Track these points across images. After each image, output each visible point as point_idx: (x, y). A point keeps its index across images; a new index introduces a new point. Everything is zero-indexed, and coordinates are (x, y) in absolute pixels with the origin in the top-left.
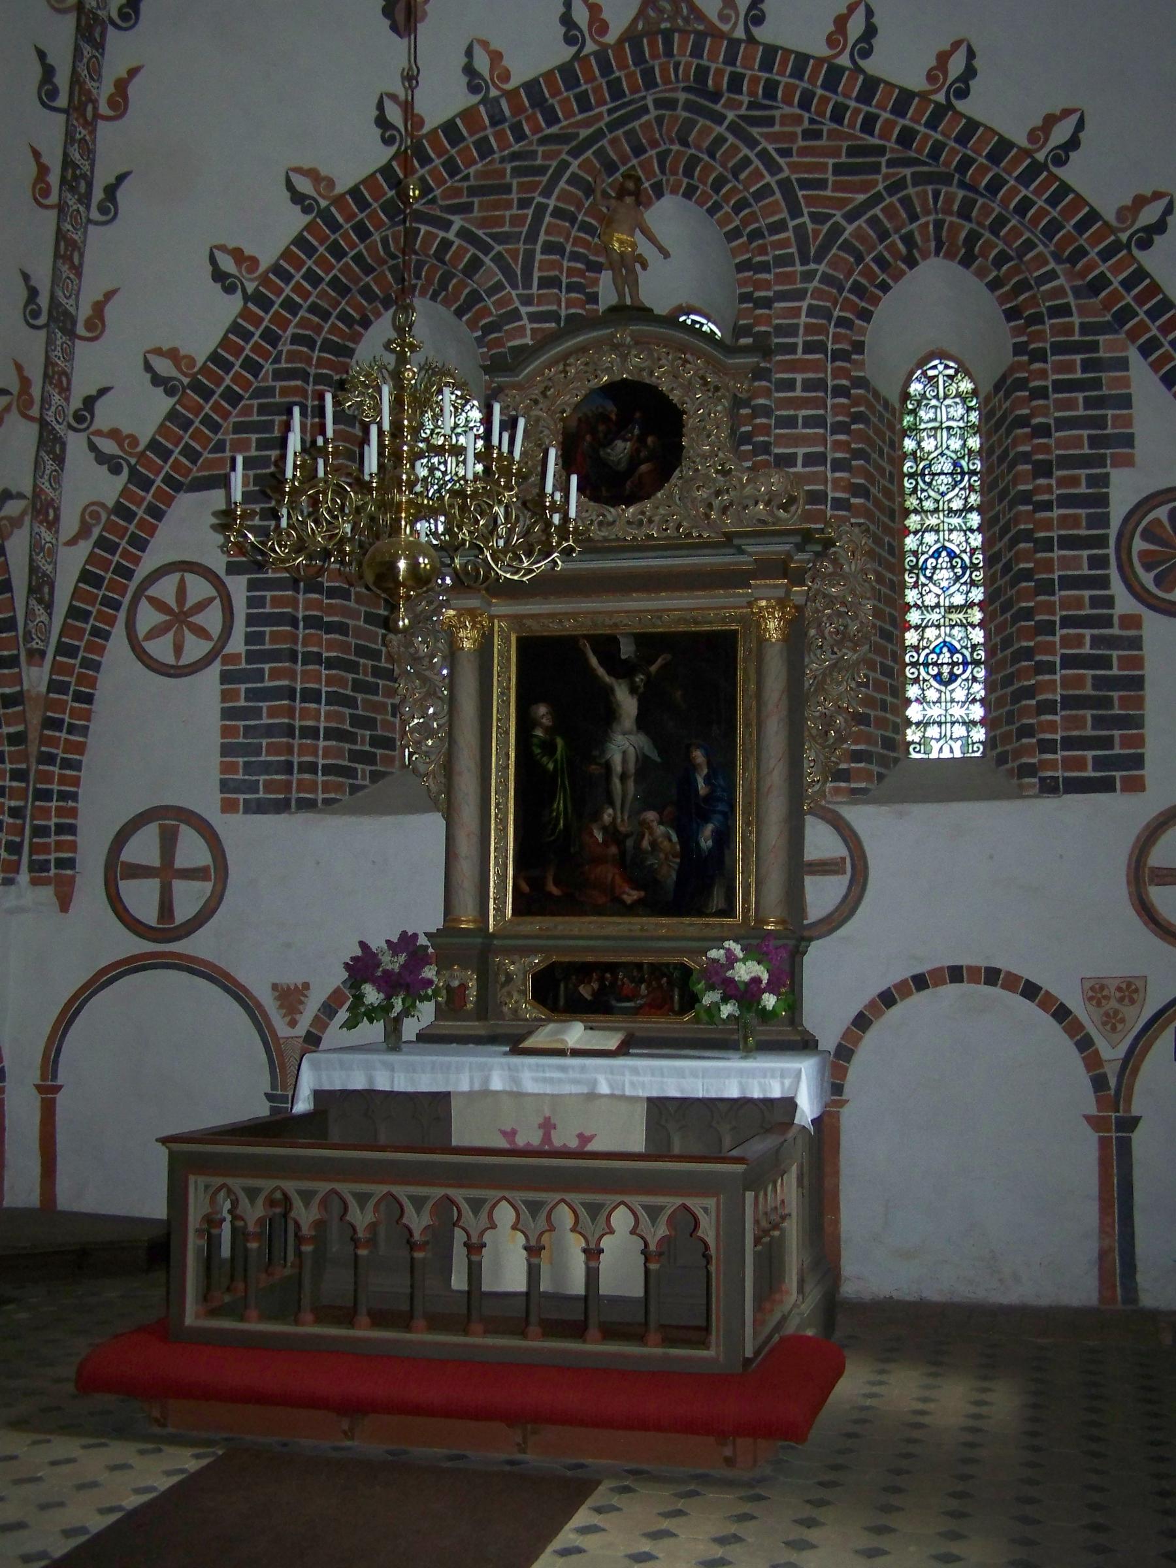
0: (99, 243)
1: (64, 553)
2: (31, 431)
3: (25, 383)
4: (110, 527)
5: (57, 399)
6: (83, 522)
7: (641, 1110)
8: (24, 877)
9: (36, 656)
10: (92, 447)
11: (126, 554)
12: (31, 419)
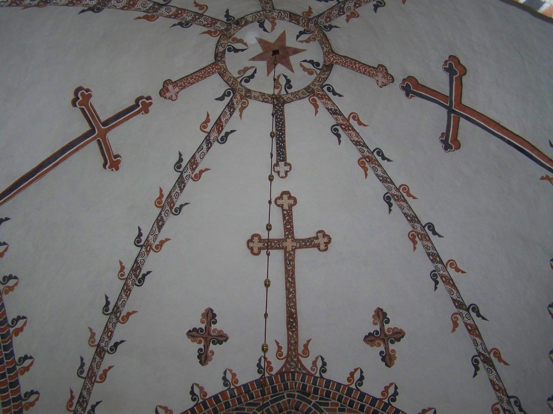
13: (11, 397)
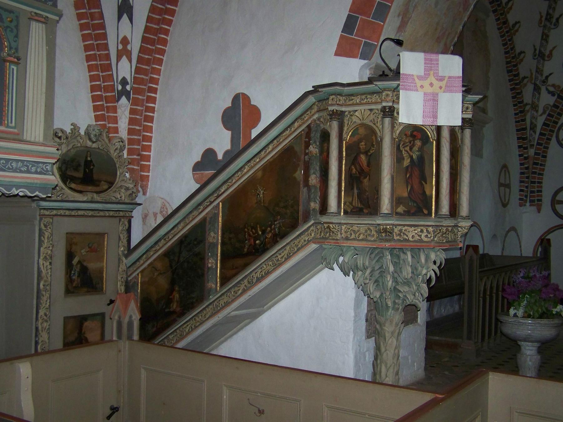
0: (553, 34)
1: (539, 118)
2: (532, 86)
3: (532, 74)
4: (552, 110)
5: (540, 78)
6: (544, 110)
7: (521, 373)
8: (528, 204)
9: (532, 146)
10: (547, 89)
11: (556, 118)
12: (532, 83)
13: (551, 124)
